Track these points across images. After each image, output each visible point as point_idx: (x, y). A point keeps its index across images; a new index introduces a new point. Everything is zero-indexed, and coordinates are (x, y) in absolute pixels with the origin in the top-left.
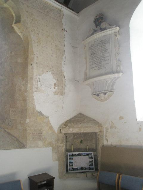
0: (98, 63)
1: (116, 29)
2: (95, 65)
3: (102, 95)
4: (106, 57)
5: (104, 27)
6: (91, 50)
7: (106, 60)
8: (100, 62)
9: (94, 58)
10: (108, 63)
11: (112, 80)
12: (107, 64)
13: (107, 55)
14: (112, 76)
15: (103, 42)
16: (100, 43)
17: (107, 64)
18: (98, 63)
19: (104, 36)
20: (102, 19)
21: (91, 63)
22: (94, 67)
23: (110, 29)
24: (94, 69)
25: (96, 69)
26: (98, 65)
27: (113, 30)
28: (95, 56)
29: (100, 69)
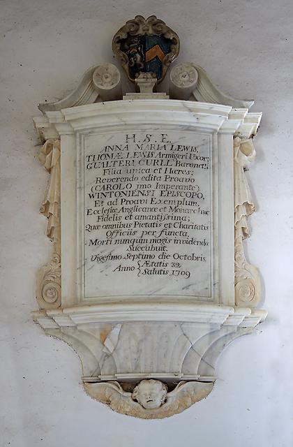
0: (141, 241)
1: (246, 120)
2: (122, 250)
3: (152, 391)
4: (195, 227)
5: (191, 85)
6: (98, 172)
7: (192, 242)
8: (156, 241)
9: (123, 215)
10: (203, 259)
11: (212, 333)
12: (193, 257)
13: (197, 219)
14: (218, 315)
15: (181, 157)
16: (163, 151)
17: (193, 257)
18: (141, 241)
19: (188, 128)
20: (143, 40)
21: (100, 234)
22: (117, 257)
23: (229, 109)
24: (116, 263)
25: (131, 269)
26: (149, 253)
27: (240, 116)
28: (129, 206)
29: (160, 272)
